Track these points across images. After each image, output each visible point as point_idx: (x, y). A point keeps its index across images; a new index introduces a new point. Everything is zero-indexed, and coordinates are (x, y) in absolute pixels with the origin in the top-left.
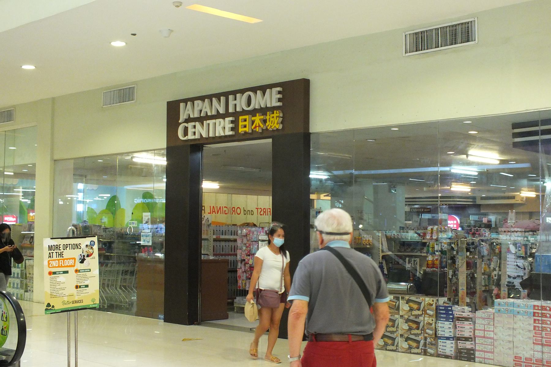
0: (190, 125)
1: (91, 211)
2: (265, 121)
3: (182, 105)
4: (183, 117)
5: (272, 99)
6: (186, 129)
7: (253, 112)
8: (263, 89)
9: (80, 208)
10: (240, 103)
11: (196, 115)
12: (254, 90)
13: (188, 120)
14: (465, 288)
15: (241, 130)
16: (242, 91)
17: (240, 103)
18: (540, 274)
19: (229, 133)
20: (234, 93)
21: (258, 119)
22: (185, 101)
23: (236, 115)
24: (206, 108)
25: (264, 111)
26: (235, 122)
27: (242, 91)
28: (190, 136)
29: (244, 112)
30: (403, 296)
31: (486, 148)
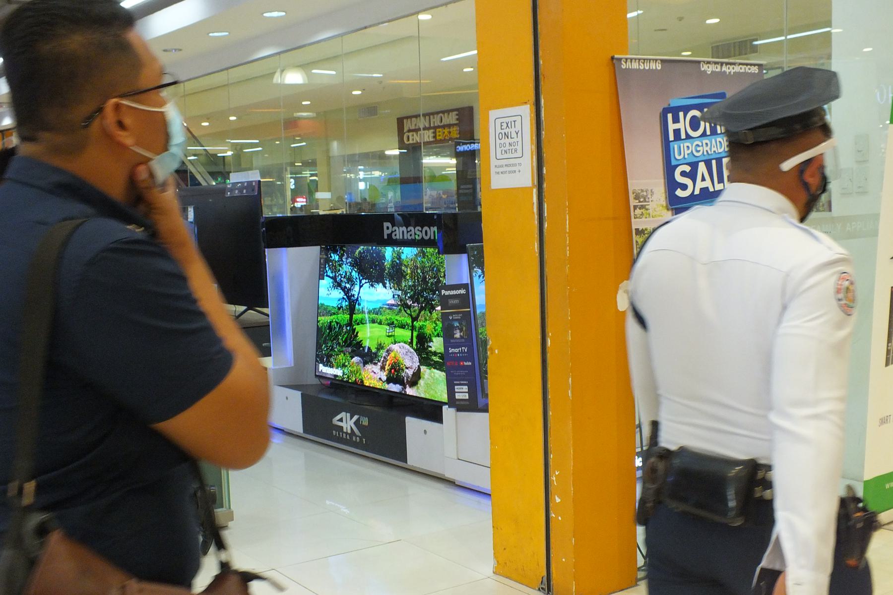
0: (410, 134)
1: (372, 188)
2: (450, 132)
3: (405, 121)
4: (406, 130)
5: (452, 119)
6: (408, 137)
7: (444, 127)
8: (448, 111)
9: (362, 186)
10: (436, 121)
11: (413, 128)
12: (443, 112)
13: (409, 131)
14: (483, 296)
15: (438, 138)
16: (438, 113)
17: (436, 121)
18: (829, 24)
19: (431, 139)
20: (433, 114)
21: (446, 131)
22: (407, 118)
23: (435, 128)
24: (703, 179)
25: (449, 126)
26: (435, 133)
27: (438, 113)
28: (411, 142)
29: (439, 127)
30: (631, 196)
31: (532, 143)
